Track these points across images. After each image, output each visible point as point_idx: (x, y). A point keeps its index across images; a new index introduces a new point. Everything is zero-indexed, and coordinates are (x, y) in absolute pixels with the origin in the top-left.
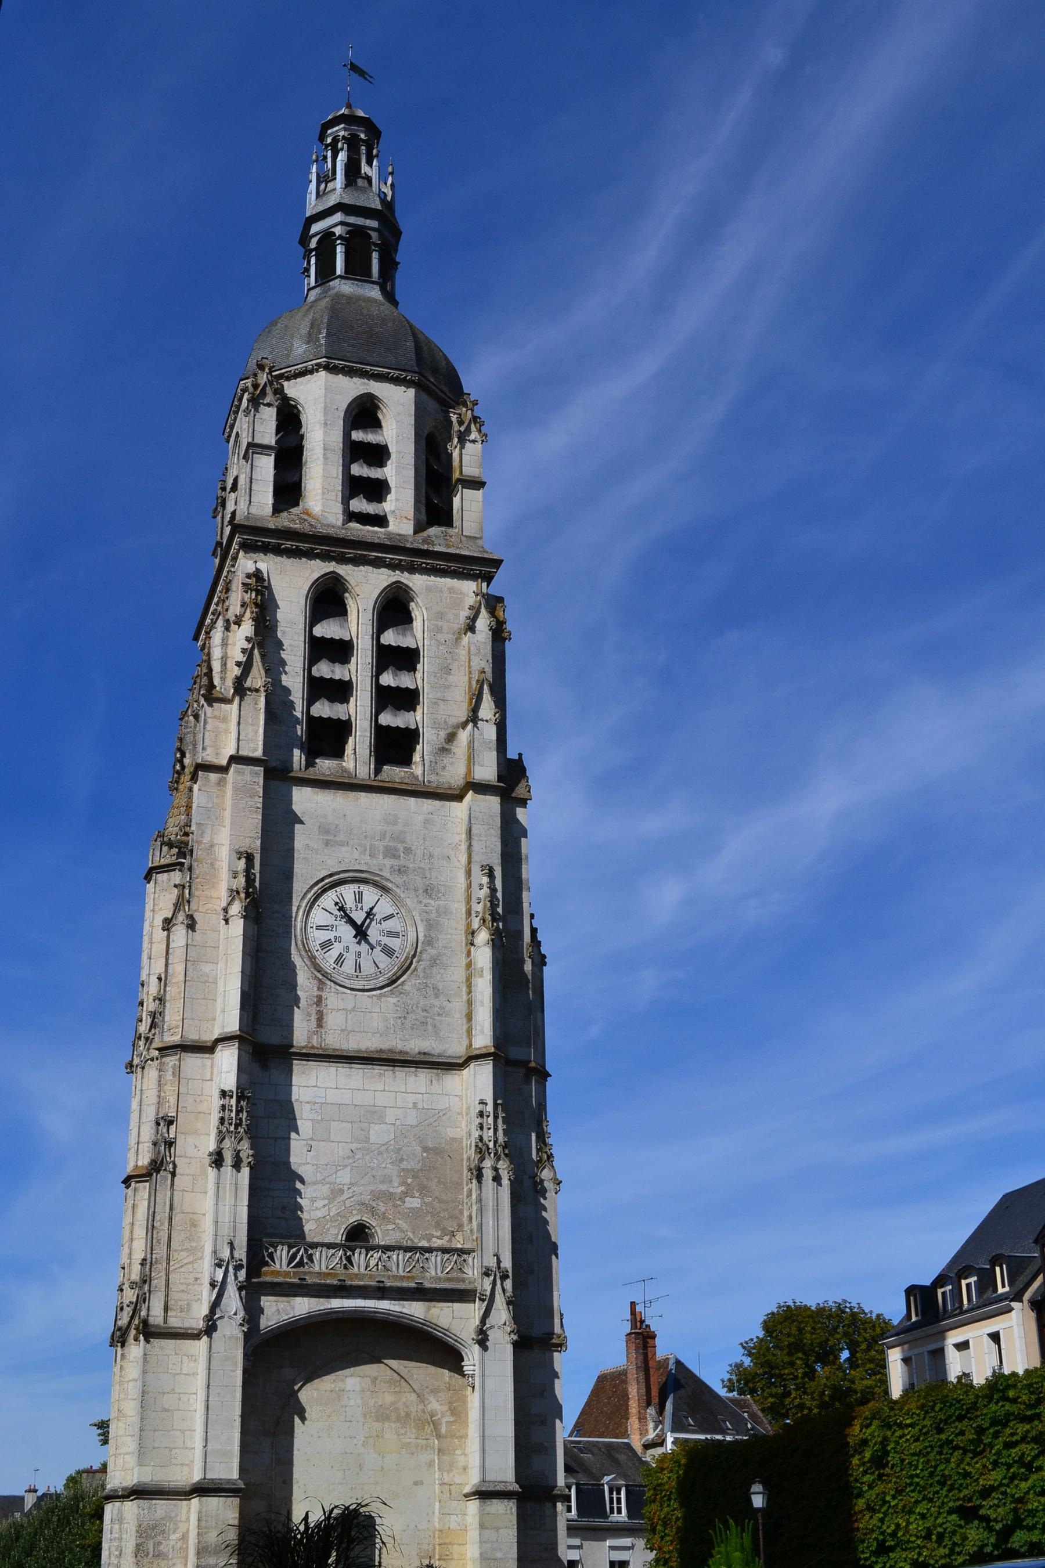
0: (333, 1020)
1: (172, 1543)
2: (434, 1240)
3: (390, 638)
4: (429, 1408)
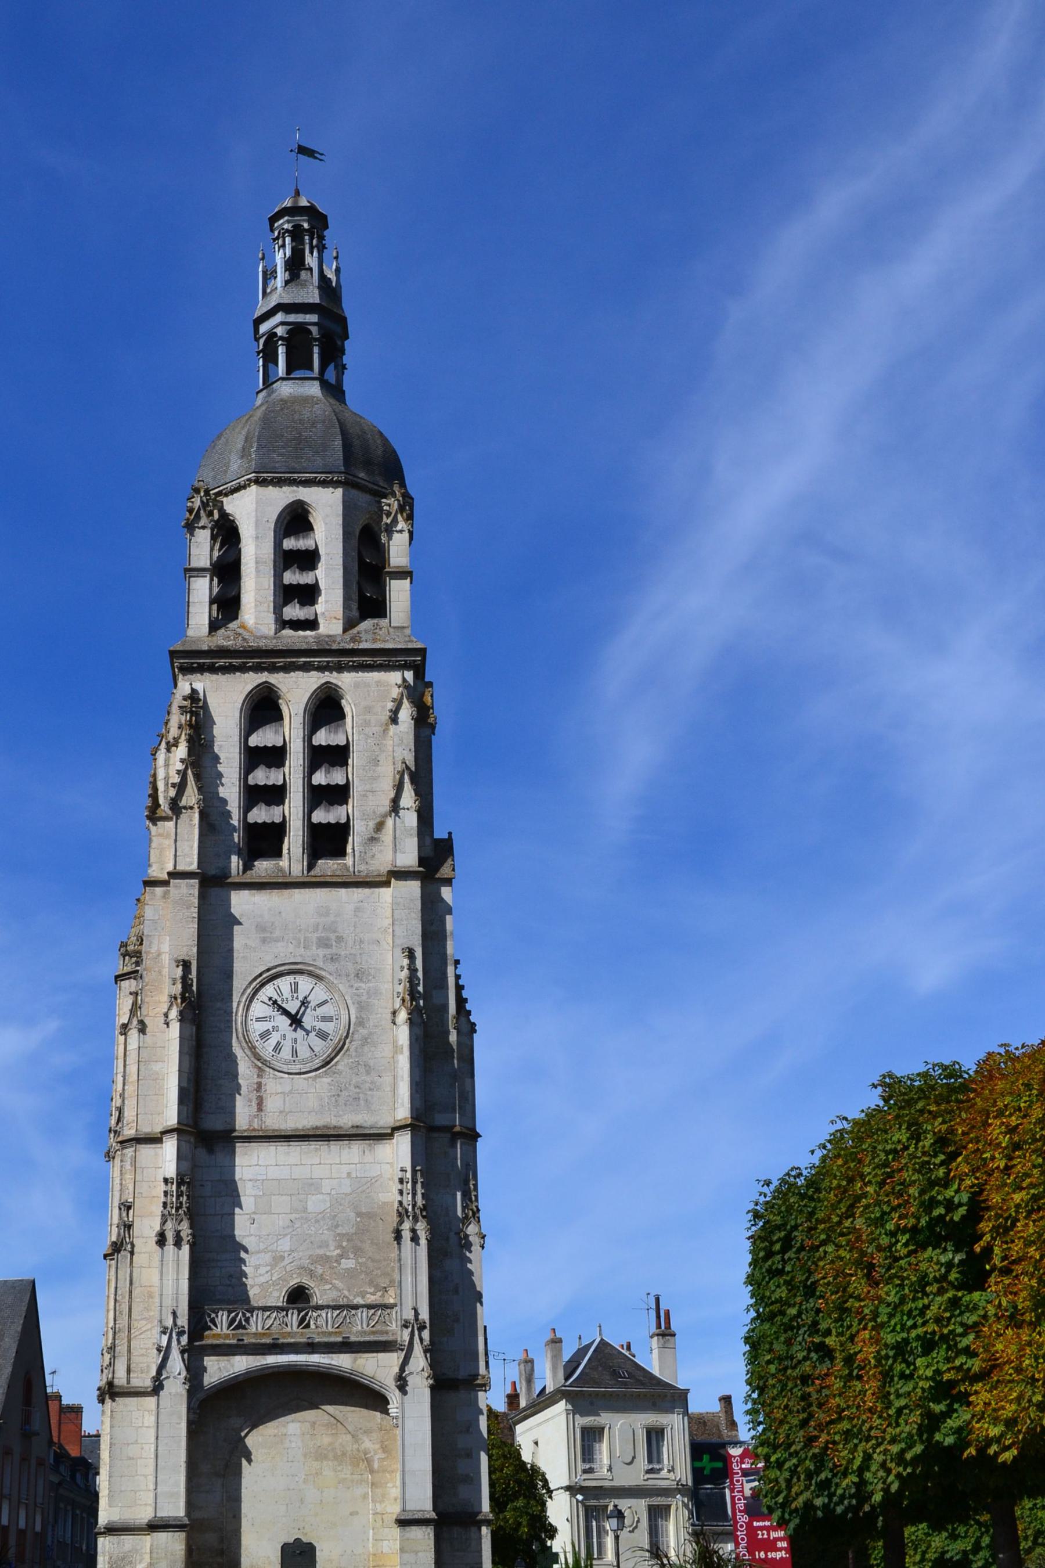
0: (272, 1104)
2: (368, 1296)
3: (323, 737)
4: (363, 1446)
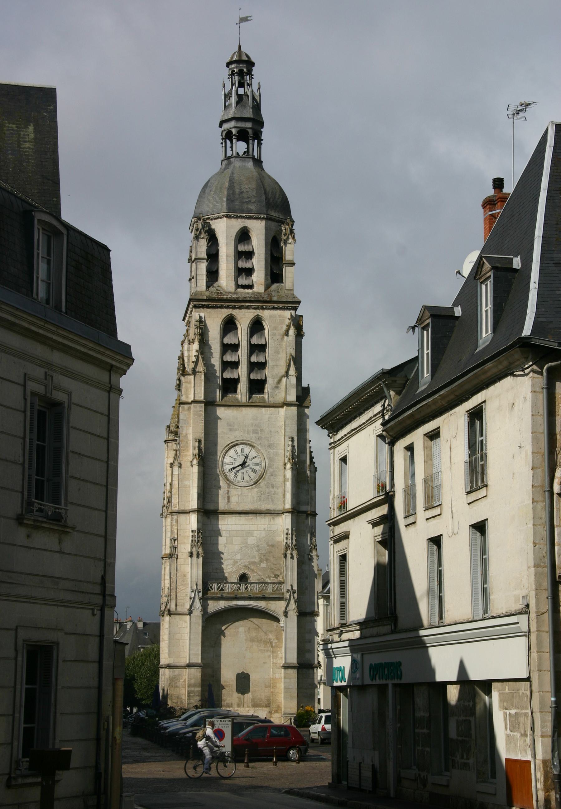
0: (234, 499)
1: (181, 683)
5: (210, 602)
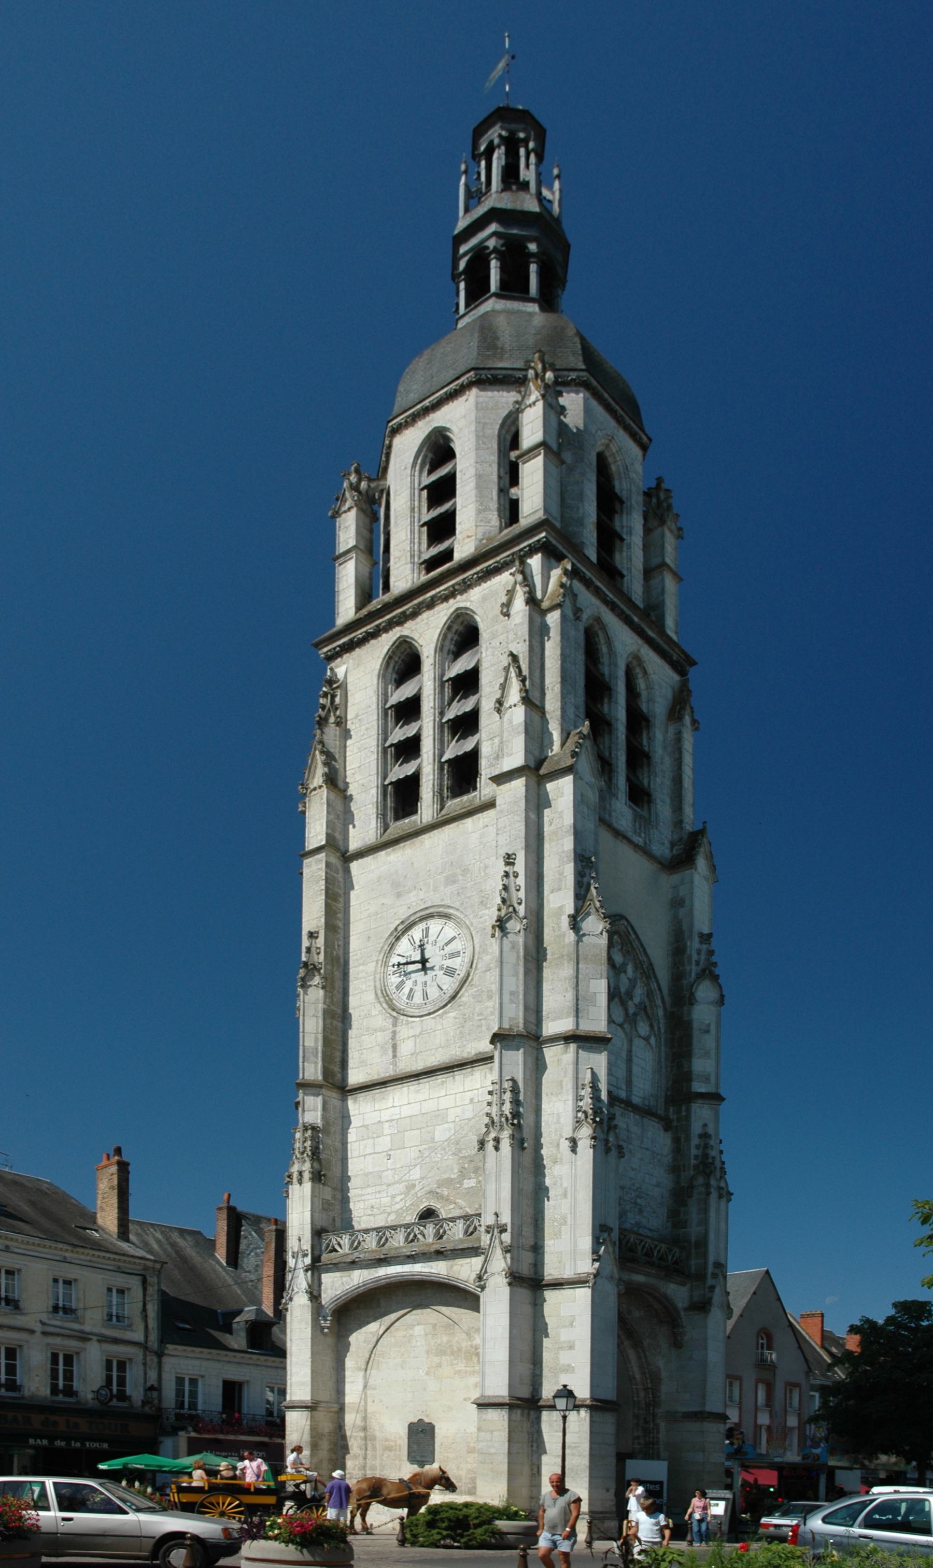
5: (326, 1278)
